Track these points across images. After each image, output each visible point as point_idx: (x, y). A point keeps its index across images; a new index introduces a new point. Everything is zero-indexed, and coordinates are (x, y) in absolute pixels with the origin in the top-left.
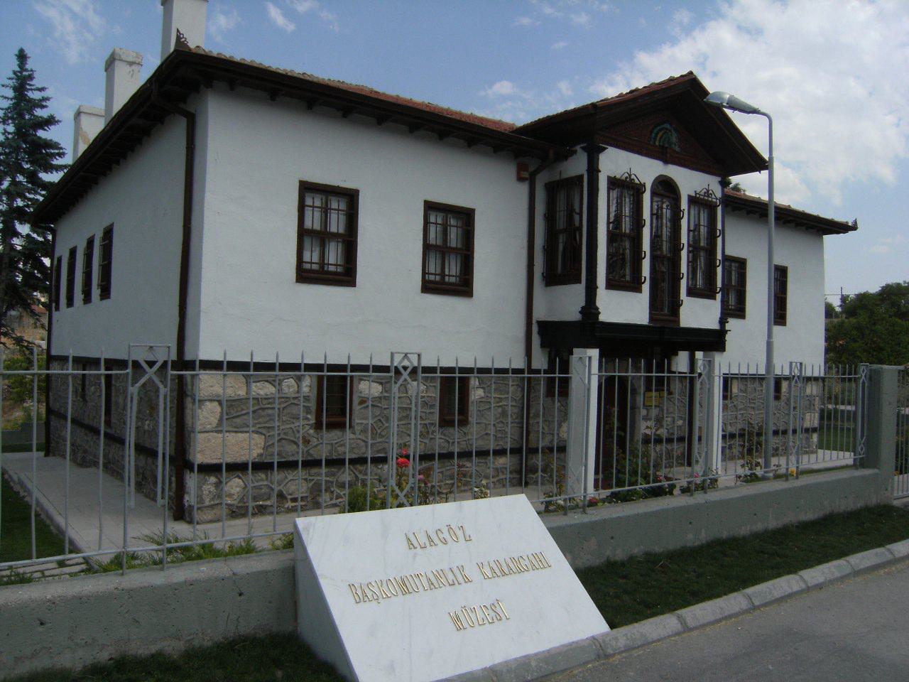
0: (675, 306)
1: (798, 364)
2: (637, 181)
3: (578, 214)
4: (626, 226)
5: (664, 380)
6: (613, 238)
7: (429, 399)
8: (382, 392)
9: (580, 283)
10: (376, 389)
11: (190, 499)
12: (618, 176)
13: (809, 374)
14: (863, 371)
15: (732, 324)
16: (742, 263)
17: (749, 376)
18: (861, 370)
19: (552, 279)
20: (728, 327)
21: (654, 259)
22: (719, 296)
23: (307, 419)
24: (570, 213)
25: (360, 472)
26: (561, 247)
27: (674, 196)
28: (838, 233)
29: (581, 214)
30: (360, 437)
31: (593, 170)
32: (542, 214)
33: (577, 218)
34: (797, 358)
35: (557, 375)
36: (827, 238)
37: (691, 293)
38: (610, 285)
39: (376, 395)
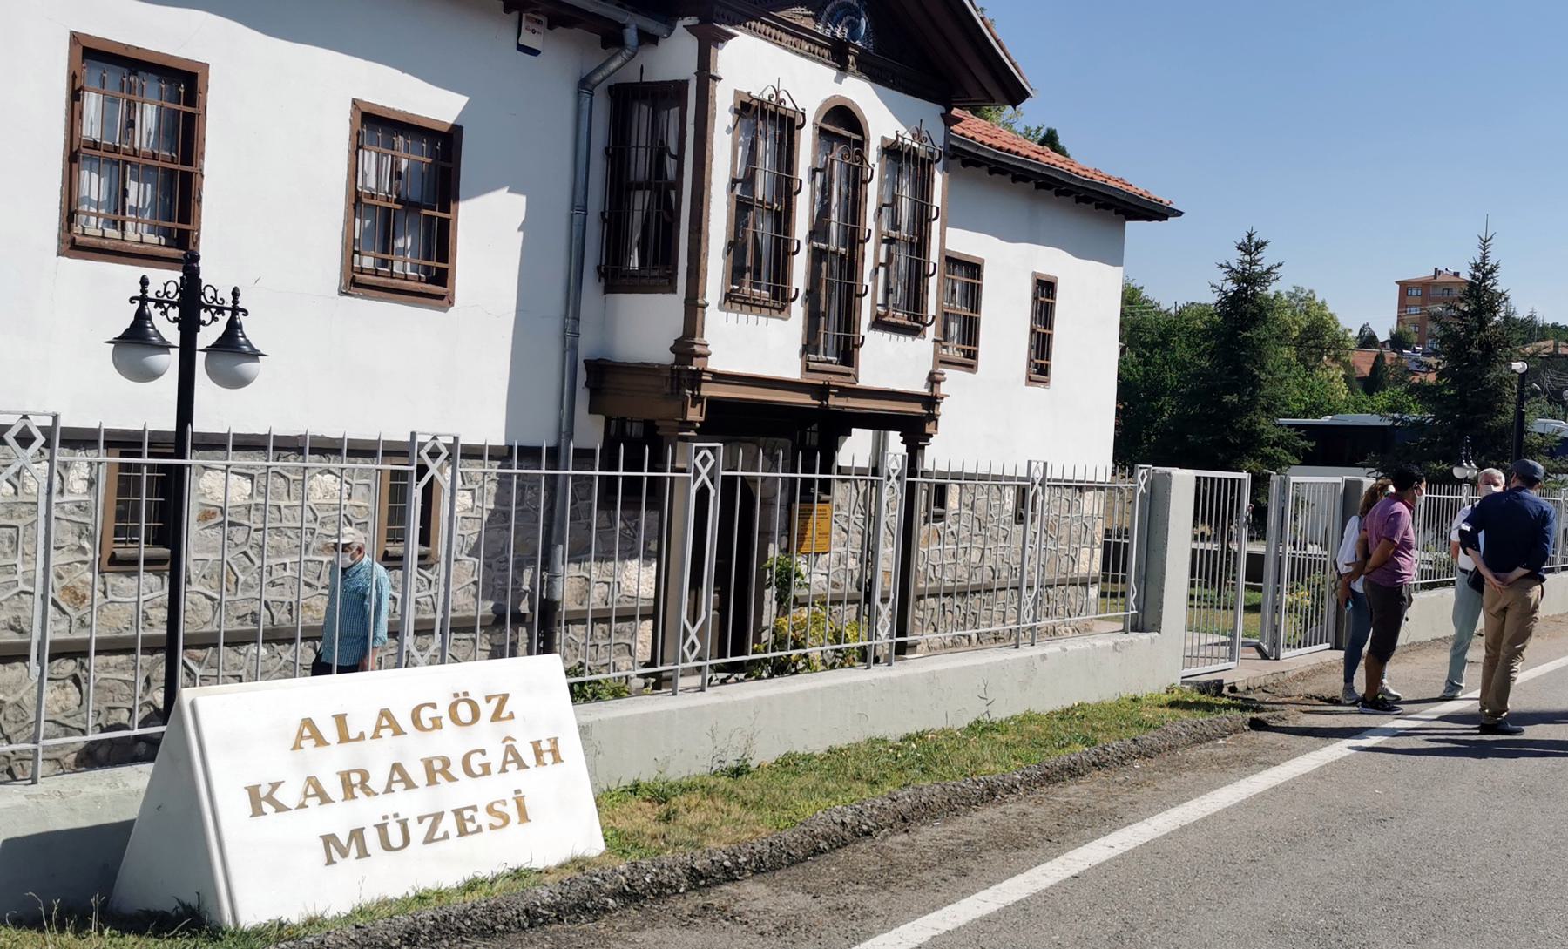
0: (847, 353)
1: (1041, 465)
2: (789, 105)
3: (672, 156)
4: (762, 189)
5: (540, 481)
6: (743, 208)
7: (354, 511)
8: (251, 496)
9: (674, 291)
10: (240, 490)
11: (62, 661)
12: (755, 94)
13: (1057, 475)
14: (1143, 476)
15: (953, 380)
16: (973, 269)
17: (1075, 484)
18: (1139, 476)
19: (615, 279)
20: (943, 389)
21: (817, 256)
22: (930, 332)
23: (82, 549)
24: (659, 153)
25: (200, 662)
26: (637, 217)
27: (858, 137)
28: (1150, 219)
29: (680, 158)
30: (201, 589)
31: (706, 76)
32: (603, 148)
33: (671, 164)
34: (1038, 456)
35: (646, 473)
36: (1131, 226)
37: (879, 324)
38: (731, 299)
39: (239, 501)
